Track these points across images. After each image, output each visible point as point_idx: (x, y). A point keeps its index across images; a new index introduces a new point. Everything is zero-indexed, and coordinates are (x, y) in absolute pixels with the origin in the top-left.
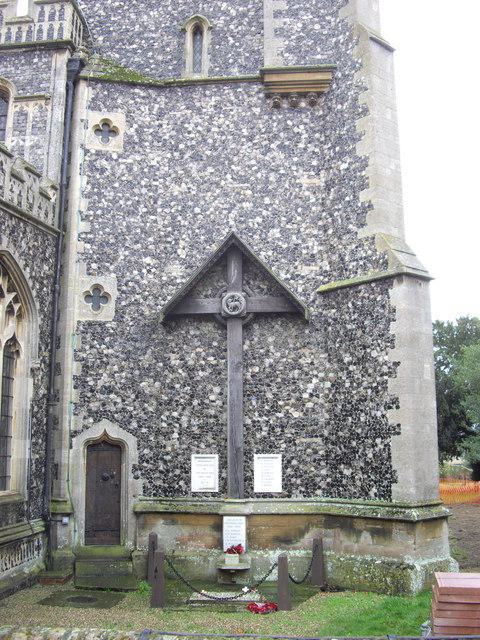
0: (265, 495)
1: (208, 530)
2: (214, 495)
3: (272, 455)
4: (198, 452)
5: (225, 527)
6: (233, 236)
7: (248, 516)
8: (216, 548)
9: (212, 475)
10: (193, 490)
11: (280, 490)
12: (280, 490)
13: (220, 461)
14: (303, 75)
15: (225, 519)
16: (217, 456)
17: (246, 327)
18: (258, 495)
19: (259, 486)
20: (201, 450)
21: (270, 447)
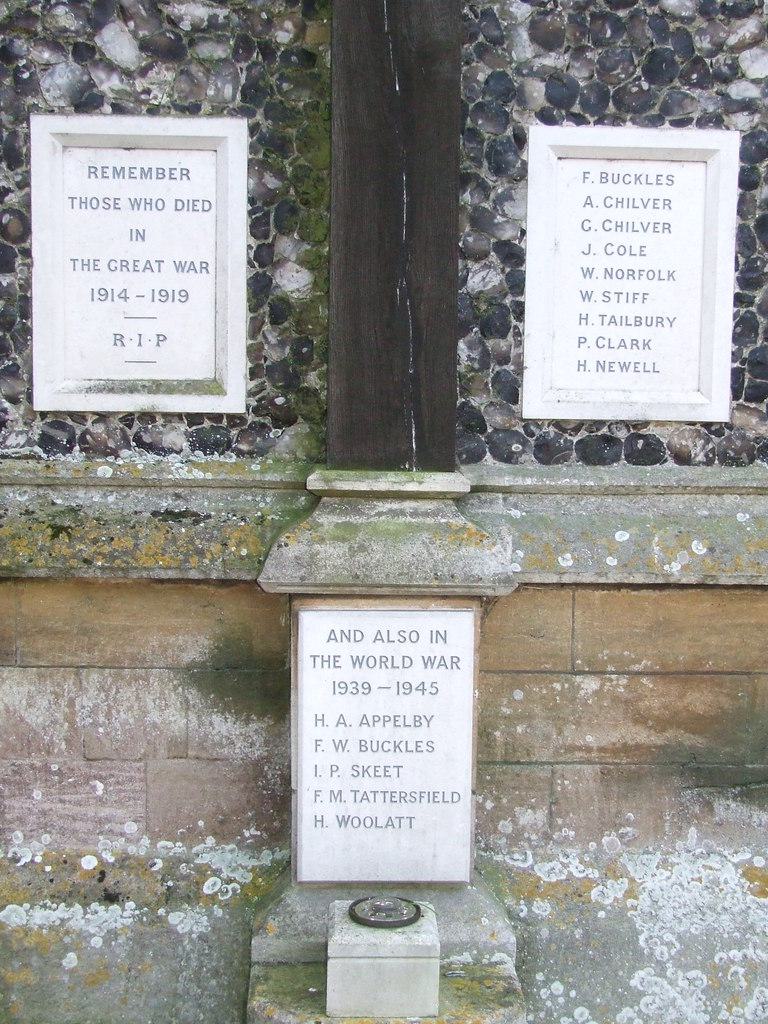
0: (601, 444)
1: (168, 711)
2: (210, 434)
3: (666, 137)
4: (85, 101)
5: (313, 690)
6: (226, 394)
7: (486, 604)
8: (223, 830)
9: (200, 286)
10: (45, 399)
11: (718, 407)
12: (718, 407)
13: (256, 167)
14: (172, 132)
15: (315, 627)
16: (235, 133)
17: (17, 436)
18: (553, 444)
19: (562, 370)
20: (109, 84)
21: (657, 68)
